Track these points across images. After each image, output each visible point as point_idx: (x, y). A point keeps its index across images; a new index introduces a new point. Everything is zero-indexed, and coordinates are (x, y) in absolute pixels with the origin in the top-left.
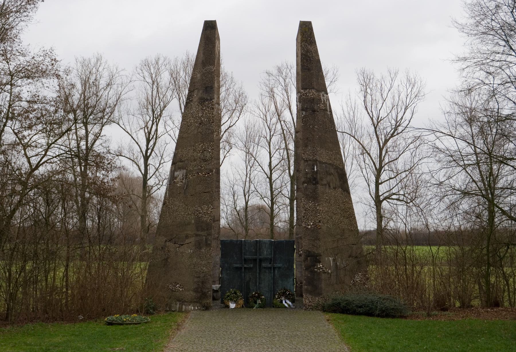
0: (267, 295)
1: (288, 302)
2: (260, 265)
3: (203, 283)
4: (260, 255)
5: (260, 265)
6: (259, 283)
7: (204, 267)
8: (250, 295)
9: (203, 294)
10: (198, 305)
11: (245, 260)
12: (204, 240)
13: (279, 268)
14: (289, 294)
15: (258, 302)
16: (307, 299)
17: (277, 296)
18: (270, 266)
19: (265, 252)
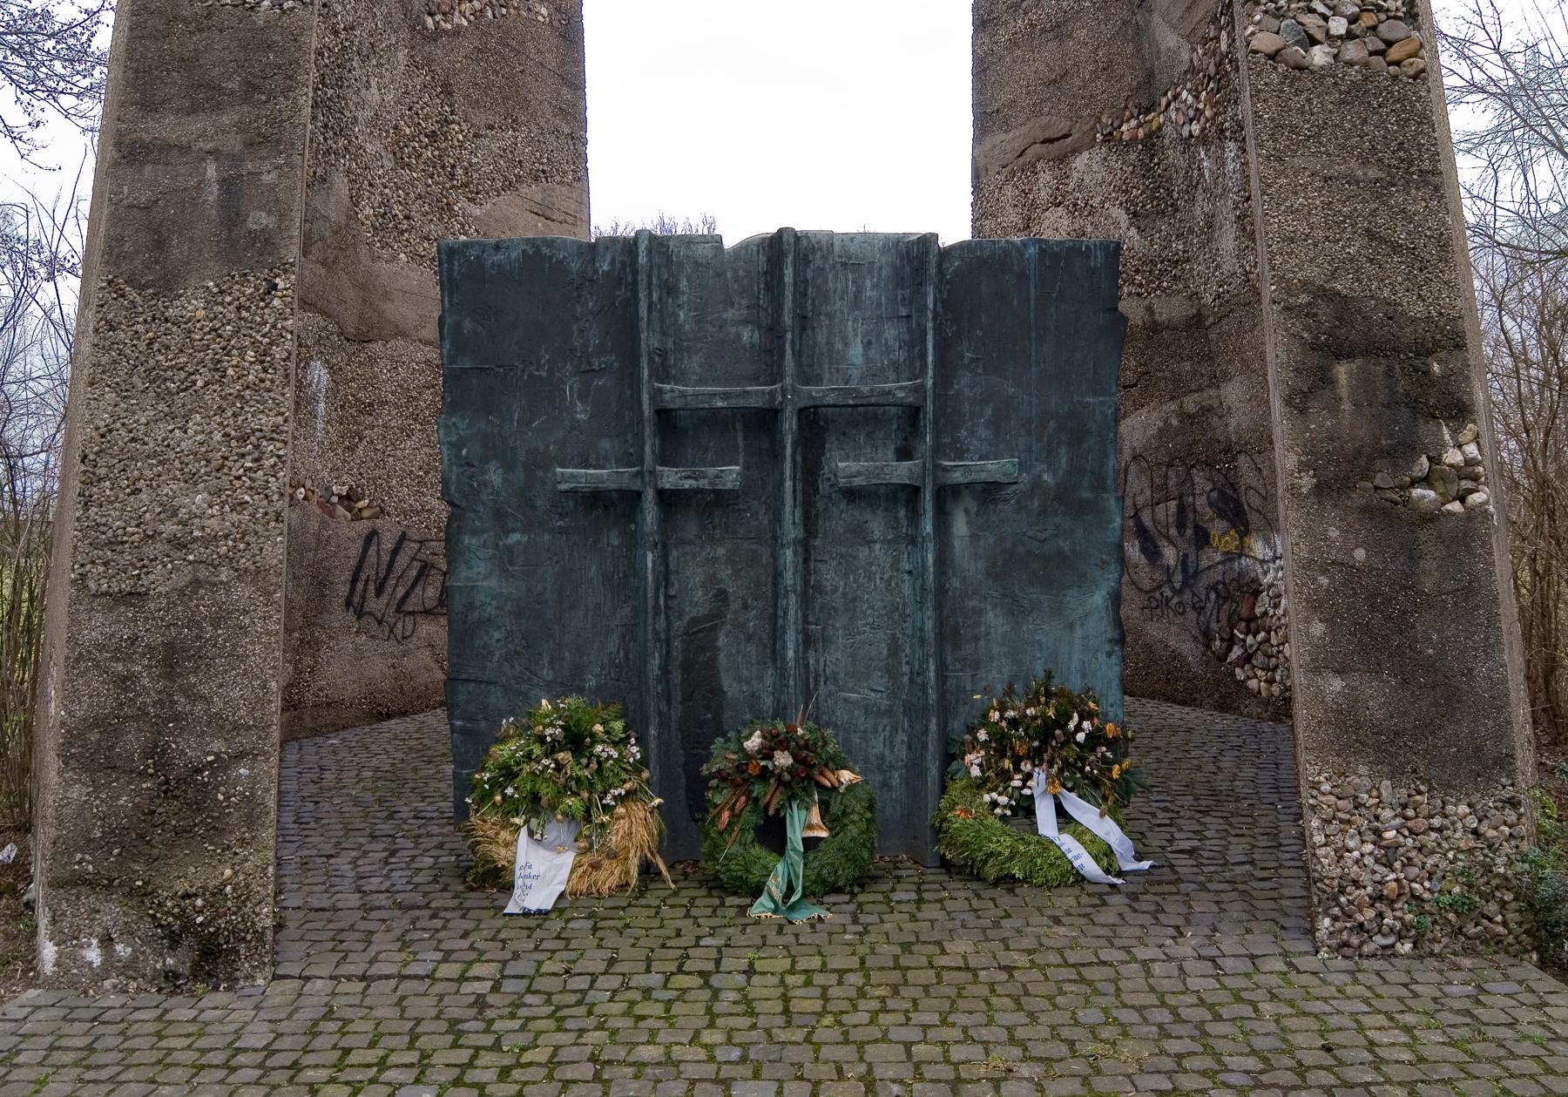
0: (877, 746)
1: (1085, 812)
2: (810, 472)
3: (171, 659)
4: (807, 377)
5: (810, 472)
6: (807, 641)
7: (192, 479)
8: (721, 758)
9: (167, 791)
10: (112, 913)
11: (666, 418)
12: (213, 194)
13: (989, 492)
14: (1095, 739)
15: (796, 835)
16: (1352, 824)
17: (974, 761)
18: (901, 472)
19: (856, 352)
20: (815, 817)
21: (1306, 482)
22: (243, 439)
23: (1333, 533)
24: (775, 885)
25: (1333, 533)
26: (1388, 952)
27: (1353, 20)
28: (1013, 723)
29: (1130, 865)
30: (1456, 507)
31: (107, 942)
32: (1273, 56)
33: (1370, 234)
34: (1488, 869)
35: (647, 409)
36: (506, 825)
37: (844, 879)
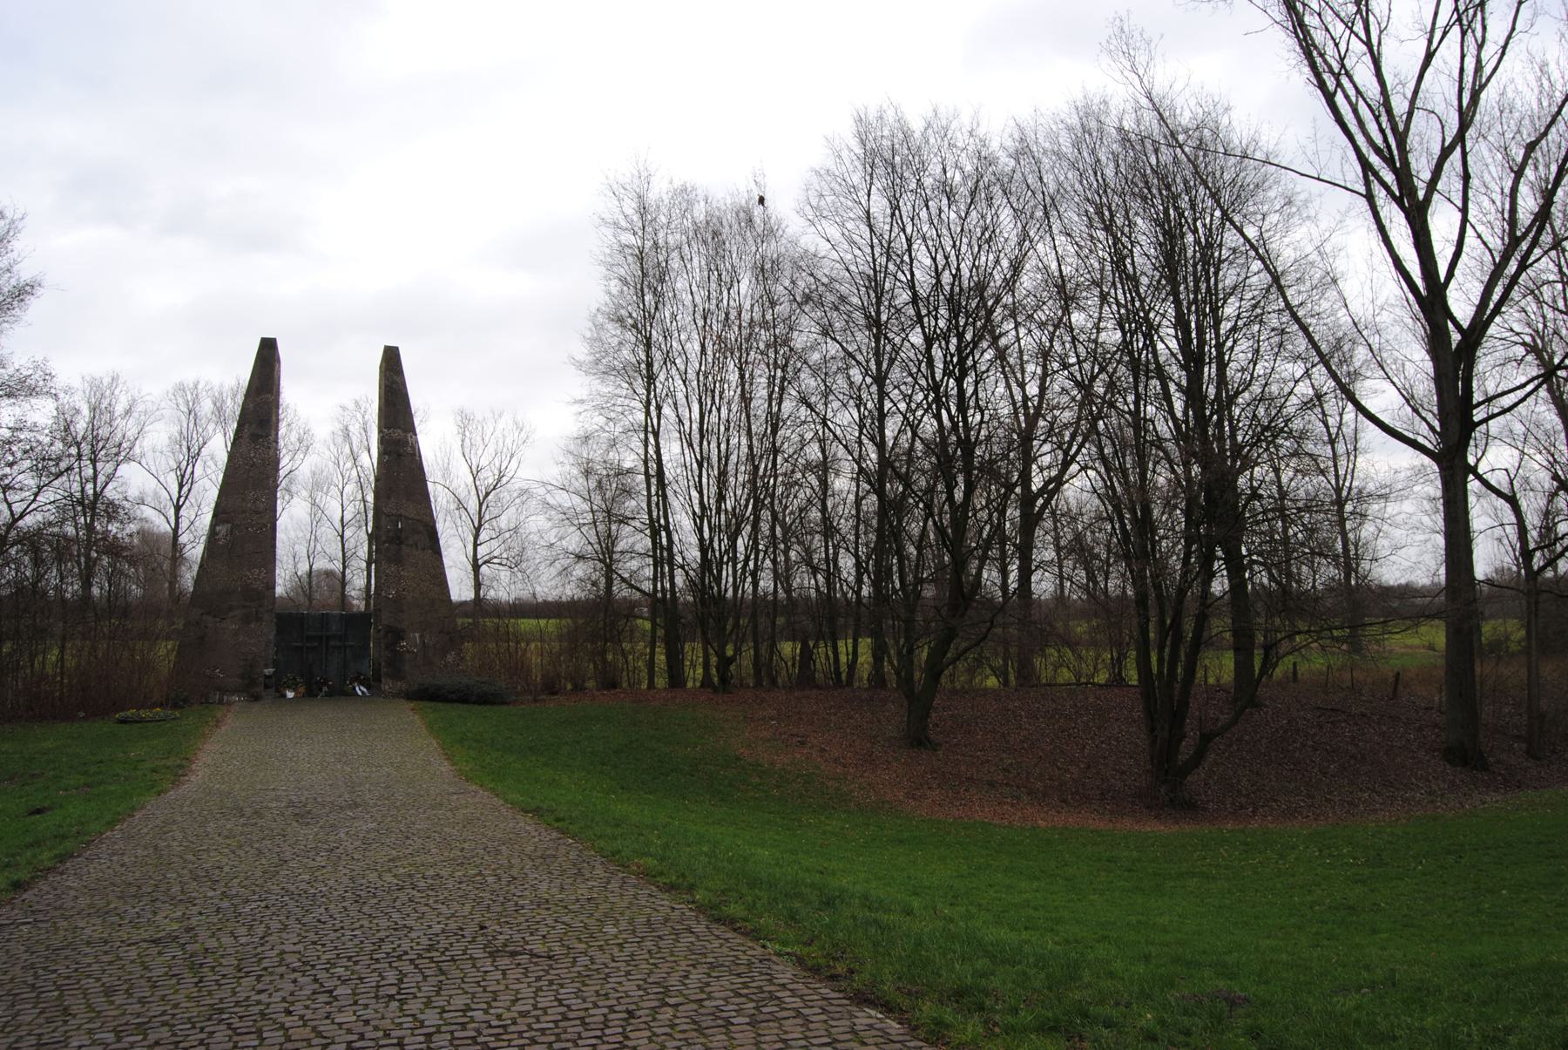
37: (330, 695)
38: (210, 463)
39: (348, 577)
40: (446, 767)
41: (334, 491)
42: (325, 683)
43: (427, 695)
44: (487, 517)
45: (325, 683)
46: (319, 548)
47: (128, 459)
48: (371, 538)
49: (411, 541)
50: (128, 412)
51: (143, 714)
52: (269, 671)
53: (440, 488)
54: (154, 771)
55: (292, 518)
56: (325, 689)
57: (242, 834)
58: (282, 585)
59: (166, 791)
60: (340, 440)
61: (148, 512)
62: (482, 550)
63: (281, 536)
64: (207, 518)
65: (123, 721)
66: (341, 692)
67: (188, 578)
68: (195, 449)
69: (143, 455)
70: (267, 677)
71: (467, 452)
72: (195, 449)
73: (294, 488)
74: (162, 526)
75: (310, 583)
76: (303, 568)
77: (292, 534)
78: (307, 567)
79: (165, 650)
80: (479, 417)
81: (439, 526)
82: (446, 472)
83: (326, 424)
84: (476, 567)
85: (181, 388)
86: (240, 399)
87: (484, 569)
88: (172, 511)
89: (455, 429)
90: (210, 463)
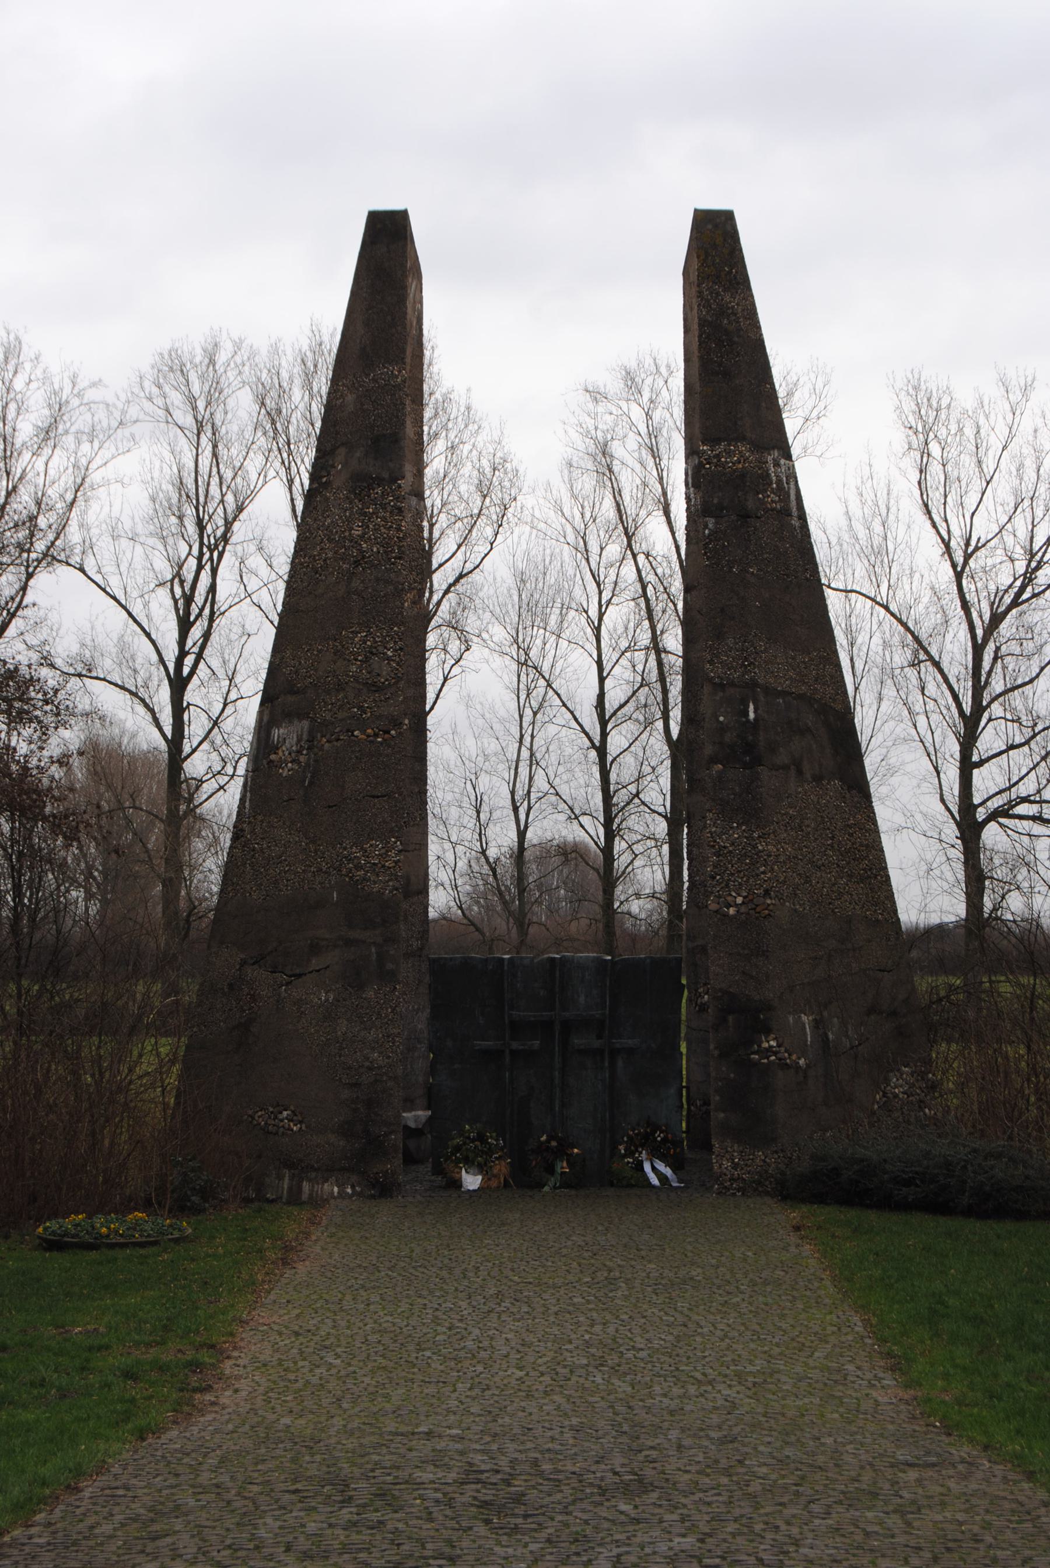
7: (373, 1049)
10: (354, 1178)
12: (374, 957)
18: (596, 1044)
20: (565, 1164)
21: (716, 1053)
22: (388, 1037)
23: (724, 1069)
24: (551, 1184)
25: (724, 1069)
26: (734, 1194)
27: (745, 897)
28: (637, 1135)
29: (675, 1184)
30: (765, 1061)
31: (353, 1187)
32: (716, 912)
33: (744, 973)
34: (766, 1172)
35: (507, 1021)
36: (457, 1167)
37: (575, 1182)
38: (255, 561)
39: (621, 862)
40: (887, 1392)
41: (578, 626)
42: (562, 1151)
43: (835, 1187)
44: (997, 685)
45: (562, 1151)
46: (541, 783)
47: (49, 557)
48: (682, 751)
49: (782, 758)
50: (48, 434)
51: (102, 1225)
52: (416, 1116)
53: (862, 605)
54: (129, 1375)
55: (469, 703)
56: (562, 1166)
57: (345, 1548)
58: (448, 885)
59: (158, 1430)
60: (587, 483)
61: (111, 701)
62: (986, 781)
63: (439, 752)
64: (247, 713)
65: (55, 1245)
66: (602, 1177)
67: (208, 870)
68: (215, 526)
69: (88, 547)
70: (410, 1133)
71: (935, 498)
72: (215, 526)
73: (471, 623)
74: (141, 732)
75: (520, 878)
76: (502, 838)
77: (471, 747)
78: (512, 836)
79: (154, 1063)
80: (965, 400)
81: (864, 719)
82: (879, 556)
83: (547, 410)
84: (970, 829)
85: (174, 366)
86: (322, 384)
87: (992, 835)
88: (163, 697)
89: (898, 438)
90: (255, 561)
